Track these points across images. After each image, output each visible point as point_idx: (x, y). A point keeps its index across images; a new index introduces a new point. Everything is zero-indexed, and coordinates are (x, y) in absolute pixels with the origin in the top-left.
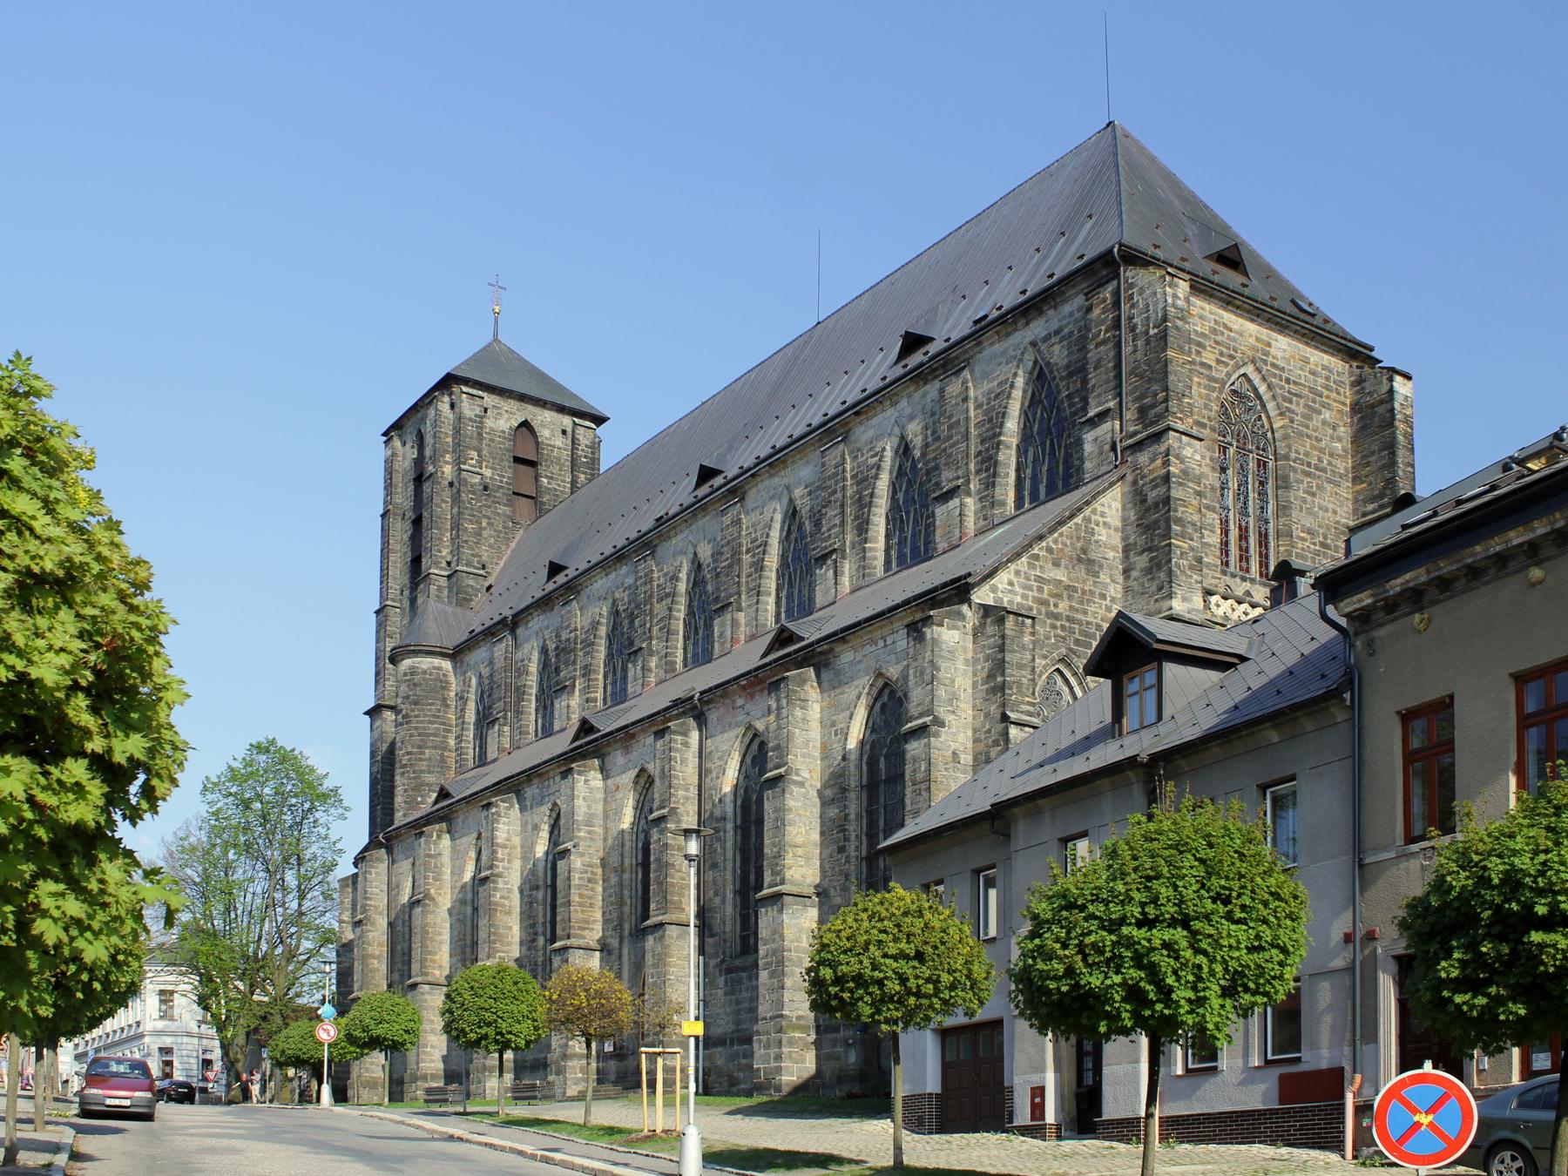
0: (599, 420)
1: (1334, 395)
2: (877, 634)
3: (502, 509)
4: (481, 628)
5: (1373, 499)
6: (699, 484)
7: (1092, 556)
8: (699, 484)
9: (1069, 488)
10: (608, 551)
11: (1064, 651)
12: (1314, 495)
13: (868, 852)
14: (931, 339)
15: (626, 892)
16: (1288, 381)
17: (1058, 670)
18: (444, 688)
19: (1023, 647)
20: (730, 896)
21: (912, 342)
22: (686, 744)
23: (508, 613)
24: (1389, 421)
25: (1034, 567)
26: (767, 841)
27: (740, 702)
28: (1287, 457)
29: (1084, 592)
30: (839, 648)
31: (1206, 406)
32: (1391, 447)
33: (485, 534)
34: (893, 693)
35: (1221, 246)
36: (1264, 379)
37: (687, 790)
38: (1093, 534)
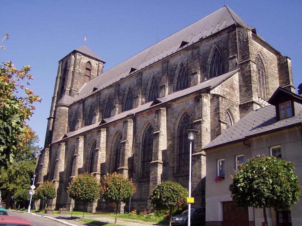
1: (274, 61)
3: (82, 78)
4: (76, 101)
6: (93, 91)
7: (233, 87)
8: (93, 91)
9: (224, 72)
10: (108, 85)
11: (228, 107)
13: (179, 153)
14: (188, 43)
15: (111, 161)
16: (266, 57)
17: (227, 112)
20: (140, 163)
25: (222, 87)
27: (145, 116)
28: (267, 72)
29: (232, 95)
30: (173, 103)
34: (187, 115)
36: (262, 55)
37: (131, 136)
38: (233, 82)
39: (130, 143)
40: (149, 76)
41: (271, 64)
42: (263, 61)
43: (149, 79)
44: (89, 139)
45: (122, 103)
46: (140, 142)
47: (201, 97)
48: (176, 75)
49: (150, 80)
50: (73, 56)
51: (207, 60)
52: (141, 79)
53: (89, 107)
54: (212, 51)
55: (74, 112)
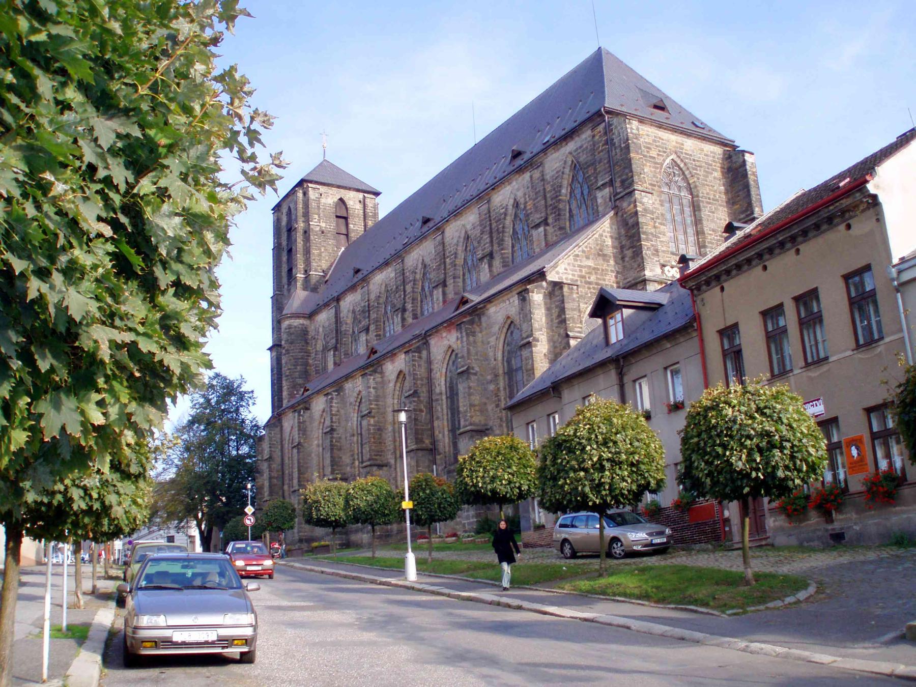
0: (377, 194)
2: (506, 298)
5: (742, 212)
12: (713, 212)
14: (525, 152)
16: (694, 160)
19: (574, 300)
20: (446, 433)
21: (517, 155)
22: (420, 357)
23: (336, 295)
24: (745, 175)
26: (461, 404)
27: (444, 335)
28: (698, 196)
31: (654, 176)
32: (747, 187)
33: (323, 255)
35: (655, 101)
36: (682, 161)
39: (422, 395)
40: (457, 234)
41: (708, 173)
42: (687, 173)
47: (528, 293)
50: (300, 194)
51: (560, 191)
52: (443, 243)
54: (567, 170)
55: (321, 330)
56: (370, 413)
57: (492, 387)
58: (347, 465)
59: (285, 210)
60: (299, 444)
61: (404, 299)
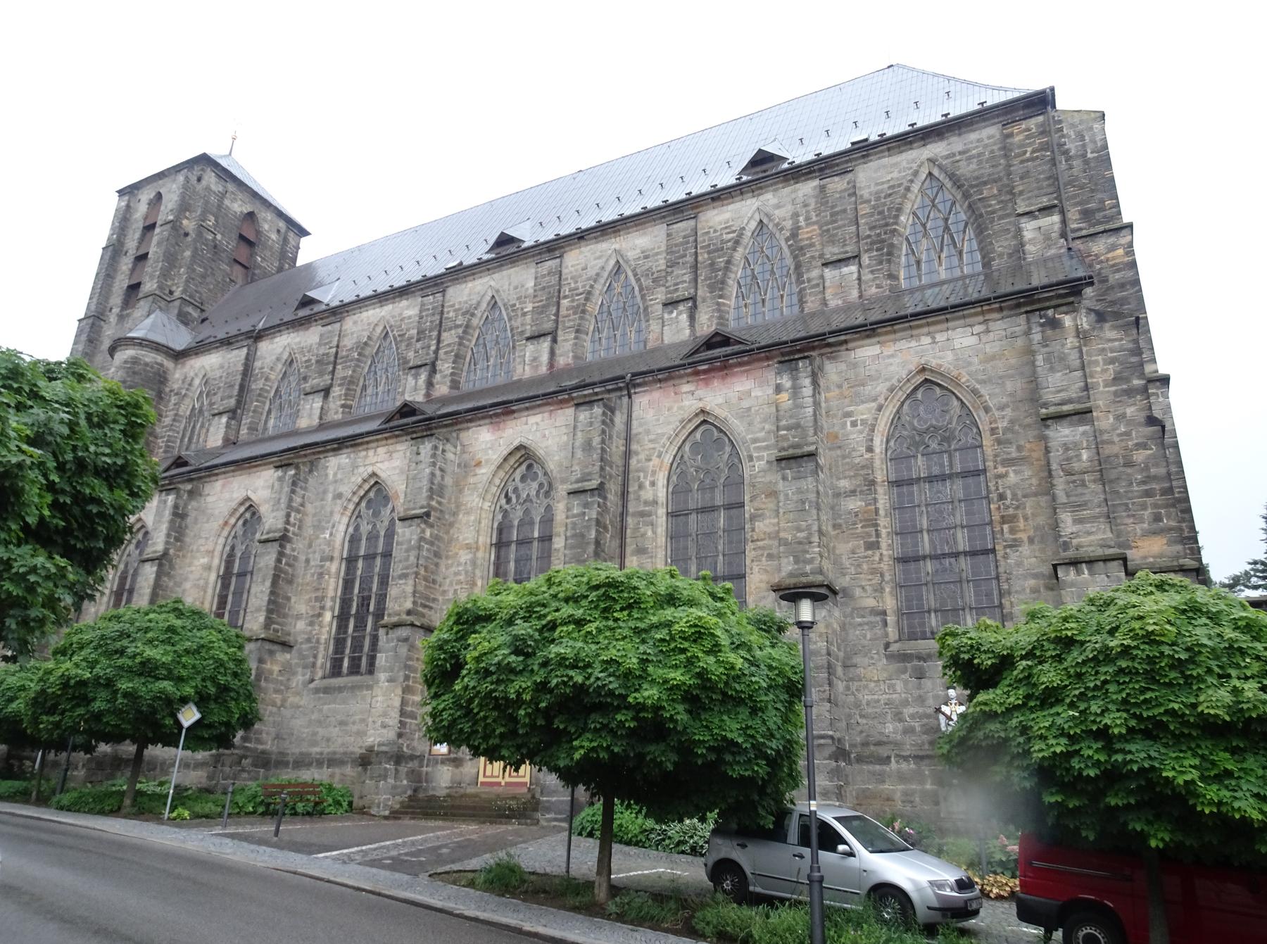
18: (161, 383)
43: (598, 275)
44: (339, 476)
45: (457, 356)
46: (655, 495)
48: (735, 269)
49: (602, 281)
51: (897, 217)
53: (280, 366)
55: (197, 382)
56: (428, 514)
57: (854, 504)
58: (299, 617)
59: (146, 196)
60: (165, 554)
61: (436, 352)
